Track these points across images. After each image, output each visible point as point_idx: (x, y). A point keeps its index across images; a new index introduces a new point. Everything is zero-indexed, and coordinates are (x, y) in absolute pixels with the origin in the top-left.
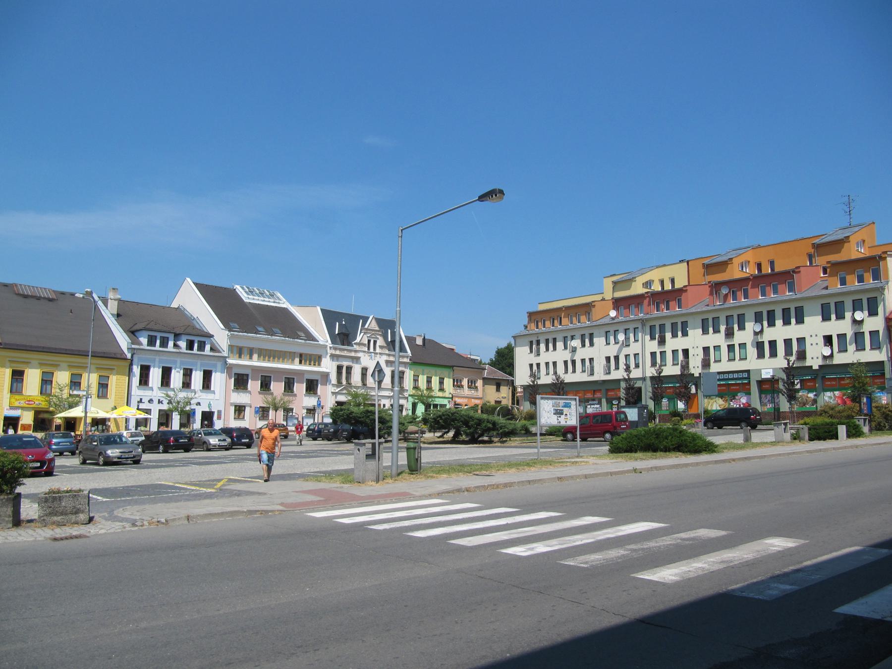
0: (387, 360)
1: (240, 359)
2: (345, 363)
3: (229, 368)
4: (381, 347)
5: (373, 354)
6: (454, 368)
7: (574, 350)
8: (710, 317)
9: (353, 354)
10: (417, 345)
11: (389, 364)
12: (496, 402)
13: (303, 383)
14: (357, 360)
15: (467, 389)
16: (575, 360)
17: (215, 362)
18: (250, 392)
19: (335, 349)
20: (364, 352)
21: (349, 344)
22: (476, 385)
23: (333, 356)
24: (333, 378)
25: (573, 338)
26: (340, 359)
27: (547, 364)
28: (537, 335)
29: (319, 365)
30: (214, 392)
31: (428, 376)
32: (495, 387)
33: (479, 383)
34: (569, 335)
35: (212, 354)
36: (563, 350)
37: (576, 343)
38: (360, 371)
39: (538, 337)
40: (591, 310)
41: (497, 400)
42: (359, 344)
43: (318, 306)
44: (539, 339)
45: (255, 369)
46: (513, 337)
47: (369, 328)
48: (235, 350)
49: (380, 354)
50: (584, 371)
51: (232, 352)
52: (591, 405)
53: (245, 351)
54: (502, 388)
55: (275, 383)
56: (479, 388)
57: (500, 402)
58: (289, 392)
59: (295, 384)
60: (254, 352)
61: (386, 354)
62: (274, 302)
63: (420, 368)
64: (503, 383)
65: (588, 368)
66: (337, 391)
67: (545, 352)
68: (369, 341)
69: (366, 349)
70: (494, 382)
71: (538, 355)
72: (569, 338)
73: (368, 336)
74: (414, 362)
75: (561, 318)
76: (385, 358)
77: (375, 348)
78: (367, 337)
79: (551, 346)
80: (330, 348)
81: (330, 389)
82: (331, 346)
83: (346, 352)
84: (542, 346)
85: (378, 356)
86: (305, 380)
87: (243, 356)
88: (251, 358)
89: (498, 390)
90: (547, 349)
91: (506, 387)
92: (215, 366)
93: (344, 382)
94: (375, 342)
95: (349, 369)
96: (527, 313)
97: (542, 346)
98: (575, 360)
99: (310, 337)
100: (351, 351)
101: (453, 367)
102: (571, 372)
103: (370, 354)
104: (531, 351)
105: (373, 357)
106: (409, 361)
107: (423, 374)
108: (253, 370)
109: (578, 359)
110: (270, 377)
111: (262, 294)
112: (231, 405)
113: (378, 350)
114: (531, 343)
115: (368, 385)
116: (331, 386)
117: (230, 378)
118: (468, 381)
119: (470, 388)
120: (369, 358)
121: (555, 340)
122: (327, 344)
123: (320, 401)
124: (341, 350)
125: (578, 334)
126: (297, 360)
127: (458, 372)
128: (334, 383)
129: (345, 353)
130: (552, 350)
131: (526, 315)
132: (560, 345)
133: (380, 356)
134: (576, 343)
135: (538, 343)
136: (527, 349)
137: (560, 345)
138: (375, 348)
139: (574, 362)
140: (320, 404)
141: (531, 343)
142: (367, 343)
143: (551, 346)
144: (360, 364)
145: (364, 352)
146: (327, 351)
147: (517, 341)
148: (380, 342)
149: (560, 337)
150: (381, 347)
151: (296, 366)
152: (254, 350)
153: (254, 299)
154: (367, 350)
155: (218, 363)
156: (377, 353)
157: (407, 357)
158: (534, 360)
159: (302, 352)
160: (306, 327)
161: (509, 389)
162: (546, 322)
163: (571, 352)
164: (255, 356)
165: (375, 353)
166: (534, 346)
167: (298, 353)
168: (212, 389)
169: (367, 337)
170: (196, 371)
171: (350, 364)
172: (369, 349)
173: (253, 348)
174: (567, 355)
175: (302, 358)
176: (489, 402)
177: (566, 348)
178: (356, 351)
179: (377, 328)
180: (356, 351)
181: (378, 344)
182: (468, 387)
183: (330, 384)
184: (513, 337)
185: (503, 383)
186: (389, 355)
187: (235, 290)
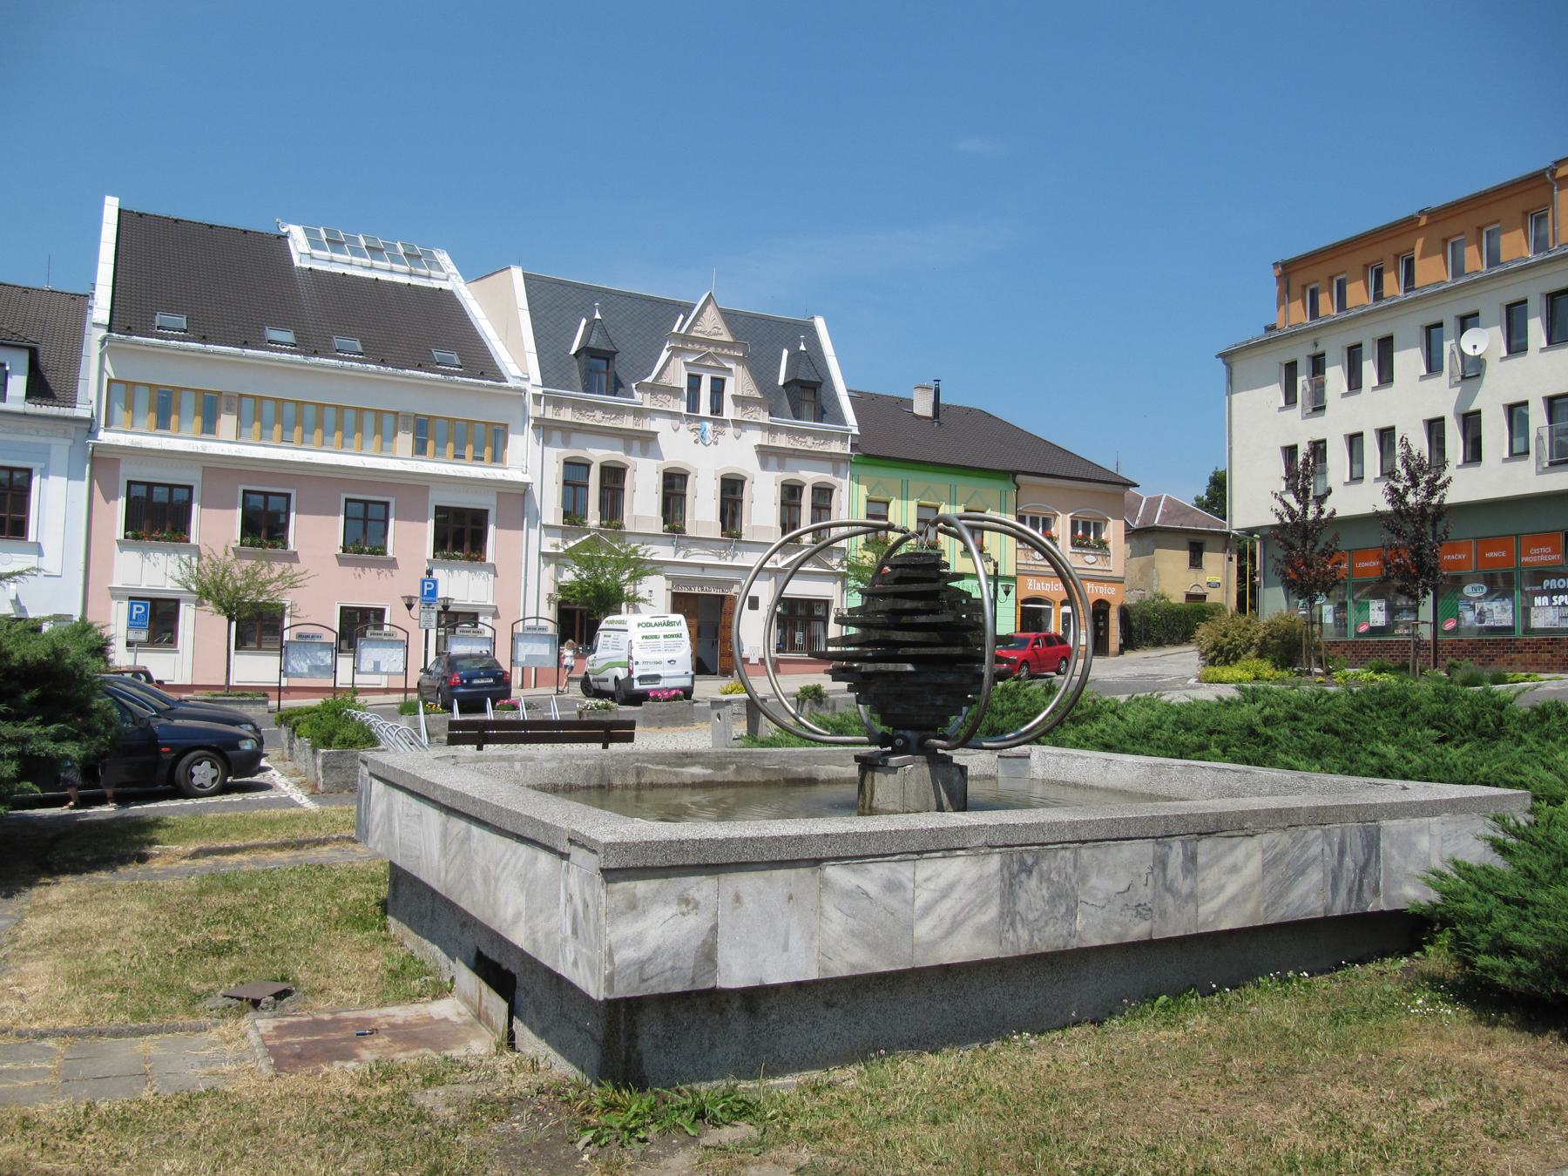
0: (760, 446)
1: (205, 436)
2: (598, 455)
3: (102, 464)
4: (740, 401)
5: (709, 426)
6: (1020, 478)
7: (1473, 370)
8: (1368, 336)
9: (628, 423)
10: (916, 416)
11: (773, 461)
12: (1189, 597)
13: (425, 520)
14: (645, 442)
15: (1070, 548)
16: (1479, 412)
17: (43, 440)
18: (493, 569)
19: (558, 403)
20: (674, 415)
21: (616, 387)
22: (1104, 536)
23: (546, 429)
24: (550, 506)
25: (1467, 321)
26: (575, 437)
27: (1354, 440)
28: (1312, 337)
29: (497, 458)
30: (38, 549)
31: (922, 502)
32: (1187, 554)
33: (1113, 531)
34: (1447, 314)
35: (31, 408)
36: (1422, 378)
37: (1484, 341)
38: (657, 482)
39: (1316, 345)
40: (1551, 202)
41: (1193, 591)
42: (655, 389)
43: (519, 264)
44: (1319, 350)
45: (217, 469)
46: (1222, 356)
47: (694, 334)
48: (142, 397)
49: (738, 423)
50: (1518, 454)
51: (129, 406)
52: (1552, 593)
53: (188, 402)
54: (1208, 557)
55: (302, 517)
56: (1110, 546)
57: (1203, 597)
58: (362, 551)
59: (392, 521)
60: (223, 406)
61: (760, 424)
62: (411, 274)
63: (892, 478)
64: (1209, 542)
65: (1539, 438)
66: (780, 565)
67: (1344, 395)
68: (695, 382)
69: (681, 407)
70: (1184, 540)
71: (1319, 408)
72: (1450, 325)
73: (690, 360)
74: (867, 456)
75: (1410, 264)
76: (757, 437)
77: (717, 408)
78: (686, 364)
79: (1369, 370)
80: (537, 398)
81: (537, 541)
82: (540, 391)
83: (599, 414)
84: (1335, 376)
85: (730, 430)
86: (123, 487)
87: (430, 445)
88: (209, 427)
89: (1196, 562)
90: (1355, 383)
91: (1221, 555)
92: (44, 453)
93: (593, 519)
94: (718, 386)
95: (614, 477)
96: (1276, 265)
97: (1335, 376)
98: (1479, 412)
99: (479, 362)
100: (620, 411)
101: (1014, 473)
102: (1460, 460)
103: (698, 425)
104: (1290, 400)
105: (709, 434)
106: (848, 451)
107: (905, 496)
108: (207, 471)
109: (1490, 404)
110: (387, 504)
111: (375, 251)
112: (114, 597)
113: (729, 411)
114: (1291, 369)
115: (690, 531)
116: (534, 533)
117: (110, 496)
118: (1074, 524)
119: (1080, 546)
120: (693, 437)
121: (1386, 347)
122: (526, 386)
123: (435, 582)
124: (577, 405)
125: (1491, 303)
126: (405, 440)
127: (1036, 496)
128: (551, 522)
129: (597, 419)
130: (1376, 383)
131: (1272, 274)
132: (1409, 360)
133: (738, 431)
134: (1484, 341)
135: (1318, 364)
136: (1276, 393)
137: (1409, 360)
138: (717, 408)
139: (1471, 423)
140: (433, 593)
141: (1291, 369)
142: (683, 383)
143: (1369, 370)
144: (659, 456)
145: (674, 415)
146: (524, 407)
147: (1235, 371)
148: (738, 382)
149: (1407, 328)
150: (740, 401)
151: (400, 459)
152: (223, 403)
153: (331, 261)
154: (684, 410)
155: (53, 441)
156: (724, 423)
157: (843, 437)
158: (1301, 430)
159: (423, 410)
160: (483, 337)
161: (1230, 559)
162: (1349, 288)
163: (1457, 384)
164: (227, 422)
165: (715, 422)
166: (1302, 381)
167: (406, 416)
168: (32, 537)
169: (686, 364)
170: (44, 474)
171: (615, 455)
172: (693, 404)
173: (220, 393)
174: (1442, 398)
175: (425, 433)
176: (1163, 598)
177: (1433, 366)
178: (640, 413)
179: (726, 337)
180: (640, 413)
181: (730, 389)
182: (1073, 544)
183: (531, 525)
184: (1220, 356)
185: (1209, 542)
186: (772, 430)
187: (285, 237)
